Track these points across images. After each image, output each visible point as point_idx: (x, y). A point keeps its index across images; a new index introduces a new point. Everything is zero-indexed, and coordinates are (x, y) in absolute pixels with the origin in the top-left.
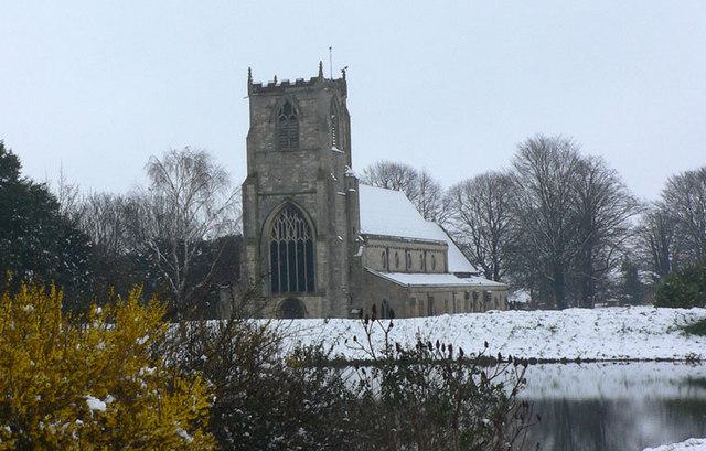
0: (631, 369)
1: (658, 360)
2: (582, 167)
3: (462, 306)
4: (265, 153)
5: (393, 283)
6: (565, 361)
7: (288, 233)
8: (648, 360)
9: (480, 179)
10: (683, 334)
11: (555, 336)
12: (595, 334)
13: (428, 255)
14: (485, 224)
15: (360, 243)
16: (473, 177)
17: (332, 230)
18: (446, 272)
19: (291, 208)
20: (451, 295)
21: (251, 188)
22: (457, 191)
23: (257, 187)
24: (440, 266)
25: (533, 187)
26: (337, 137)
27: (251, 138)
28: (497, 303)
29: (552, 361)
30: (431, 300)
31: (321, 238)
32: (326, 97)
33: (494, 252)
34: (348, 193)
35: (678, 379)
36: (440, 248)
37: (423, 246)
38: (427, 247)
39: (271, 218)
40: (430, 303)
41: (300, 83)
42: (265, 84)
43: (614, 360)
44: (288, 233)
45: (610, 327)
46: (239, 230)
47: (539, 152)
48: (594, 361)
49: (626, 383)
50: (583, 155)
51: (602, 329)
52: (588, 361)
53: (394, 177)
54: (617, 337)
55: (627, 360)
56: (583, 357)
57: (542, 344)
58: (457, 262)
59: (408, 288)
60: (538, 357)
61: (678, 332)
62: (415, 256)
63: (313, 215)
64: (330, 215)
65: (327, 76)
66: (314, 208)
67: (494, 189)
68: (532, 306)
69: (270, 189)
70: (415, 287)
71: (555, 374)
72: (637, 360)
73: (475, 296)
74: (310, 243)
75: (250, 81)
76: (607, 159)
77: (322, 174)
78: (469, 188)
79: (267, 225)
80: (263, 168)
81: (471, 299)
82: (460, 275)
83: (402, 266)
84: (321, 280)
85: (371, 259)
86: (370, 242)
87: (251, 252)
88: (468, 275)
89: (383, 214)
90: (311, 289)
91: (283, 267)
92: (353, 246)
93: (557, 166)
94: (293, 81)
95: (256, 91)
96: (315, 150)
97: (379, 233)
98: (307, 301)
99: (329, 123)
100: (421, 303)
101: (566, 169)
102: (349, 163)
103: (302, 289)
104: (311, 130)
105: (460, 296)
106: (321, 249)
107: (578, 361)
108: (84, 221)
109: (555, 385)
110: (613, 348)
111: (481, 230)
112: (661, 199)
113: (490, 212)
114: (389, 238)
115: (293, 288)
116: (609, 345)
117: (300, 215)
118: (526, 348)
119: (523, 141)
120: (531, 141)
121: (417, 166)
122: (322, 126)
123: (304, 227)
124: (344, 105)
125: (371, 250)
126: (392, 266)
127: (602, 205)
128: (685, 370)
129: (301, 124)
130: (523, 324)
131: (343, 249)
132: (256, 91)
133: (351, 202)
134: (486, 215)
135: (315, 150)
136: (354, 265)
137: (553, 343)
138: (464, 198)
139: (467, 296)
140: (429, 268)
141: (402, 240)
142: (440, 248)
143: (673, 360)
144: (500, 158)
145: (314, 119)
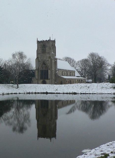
0: (103, 95)
1: (108, 94)
2: (100, 58)
3: (77, 82)
4: (40, 53)
5: (63, 78)
6: (90, 94)
7: (44, 68)
8: (106, 94)
9: (82, 60)
10: (113, 89)
11: (89, 89)
12: (97, 88)
13: (71, 73)
14: (83, 68)
15: (57, 70)
16: (81, 59)
17: (51, 68)
18: (75, 76)
19: (44, 63)
20: (74, 80)
21: (37, 60)
22: (78, 62)
23: (38, 60)
24: (73, 75)
25: (91, 61)
26: (53, 51)
27: (37, 51)
28: (84, 82)
29: (88, 94)
30: (70, 81)
31: (49, 69)
32: (51, 43)
33: (85, 73)
34: (55, 61)
35: (112, 97)
36: (74, 72)
37: (70, 71)
38: (71, 71)
39: (40, 66)
40: (70, 82)
41: (46, 41)
42: (40, 41)
43: (100, 94)
44: (44, 68)
45: (100, 87)
46: (34, 66)
47: (92, 55)
48: (96, 94)
49: (102, 98)
50: (100, 56)
51: (98, 87)
52: (95, 94)
53: (68, 60)
54: (101, 89)
55: (102, 94)
56: (94, 93)
57: (86, 90)
58: (77, 74)
59: (66, 79)
60: (85, 93)
61: (112, 88)
62: (69, 73)
63: (48, 65)
64: (51, 65)
65: (51, 39)
66: (48, 63)
67: (85, 61)
68: (92, 82)
69: (40, 60)
70: (67, 78)
71: (88, 96)
72: (104, 94)
73: (80, 80)
74: (48, 71)
75: (37, 40)
76: (104, 57)
77: (50, 57)
78: (80, 61)
79: (40, 66)
80: (39, 56)
81: (79, 81)
82: (77, 77)
83: (66, 75)
84: (49, 77)
85: (59, 74)
86: (59, 70)
87: (37, 72)
88: (79, 77)
89: (62, 65)
90: (47, 79)
91: (43, 75)
92: (56, 71)
93: (95, 57)
94: (45, 40)
95: (38, 42)
96: (49, 53)
97: (60, 69)
98: (47, 81)
99: (52, 48)
100: (68, 82)
101: (97, 58)
102: (56, 56)
103: (46, 79)
104: (48, 49)
105: (77, 80)
106: (49, 71)
107: (92, 94)
108: (13, 67)
109: (89, 98)
110: (100, 91)
111: (83, 69)
112: (114, 64)
113: (84, 66)
114: (63, 70)
115: (44, 78)
116: (99, 90)
117: (46, 65)
118: (83, 91)
119: (90, 53)
120: (91, 53)
121: (72, 57)
122: (50, 49)
123: (47, 67)
124: (55, 45)
125: (59, 72)
126: (64, 75)
127: (103, 65)
128: (113, 96)
129: (46, 48)
130: (83, 86)
131: (54, 71)
132: (38, 42)
133: (56, 63)
134: (83, 66)
135: (49, 53)
136: (56, 75)
137: (88, 90)
138: (80, 63)
139: (78, 80)
140: (71, 75)
141: (66, 70)
142: (74, 72)
143: (111, 94)
144: (86, 56)
145: (48, 47)
